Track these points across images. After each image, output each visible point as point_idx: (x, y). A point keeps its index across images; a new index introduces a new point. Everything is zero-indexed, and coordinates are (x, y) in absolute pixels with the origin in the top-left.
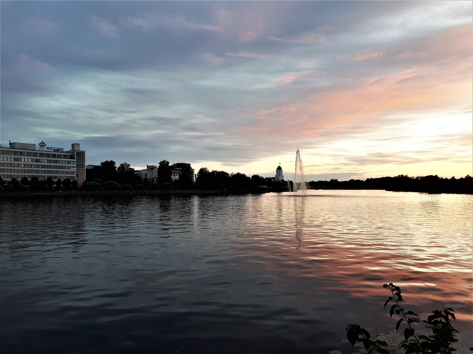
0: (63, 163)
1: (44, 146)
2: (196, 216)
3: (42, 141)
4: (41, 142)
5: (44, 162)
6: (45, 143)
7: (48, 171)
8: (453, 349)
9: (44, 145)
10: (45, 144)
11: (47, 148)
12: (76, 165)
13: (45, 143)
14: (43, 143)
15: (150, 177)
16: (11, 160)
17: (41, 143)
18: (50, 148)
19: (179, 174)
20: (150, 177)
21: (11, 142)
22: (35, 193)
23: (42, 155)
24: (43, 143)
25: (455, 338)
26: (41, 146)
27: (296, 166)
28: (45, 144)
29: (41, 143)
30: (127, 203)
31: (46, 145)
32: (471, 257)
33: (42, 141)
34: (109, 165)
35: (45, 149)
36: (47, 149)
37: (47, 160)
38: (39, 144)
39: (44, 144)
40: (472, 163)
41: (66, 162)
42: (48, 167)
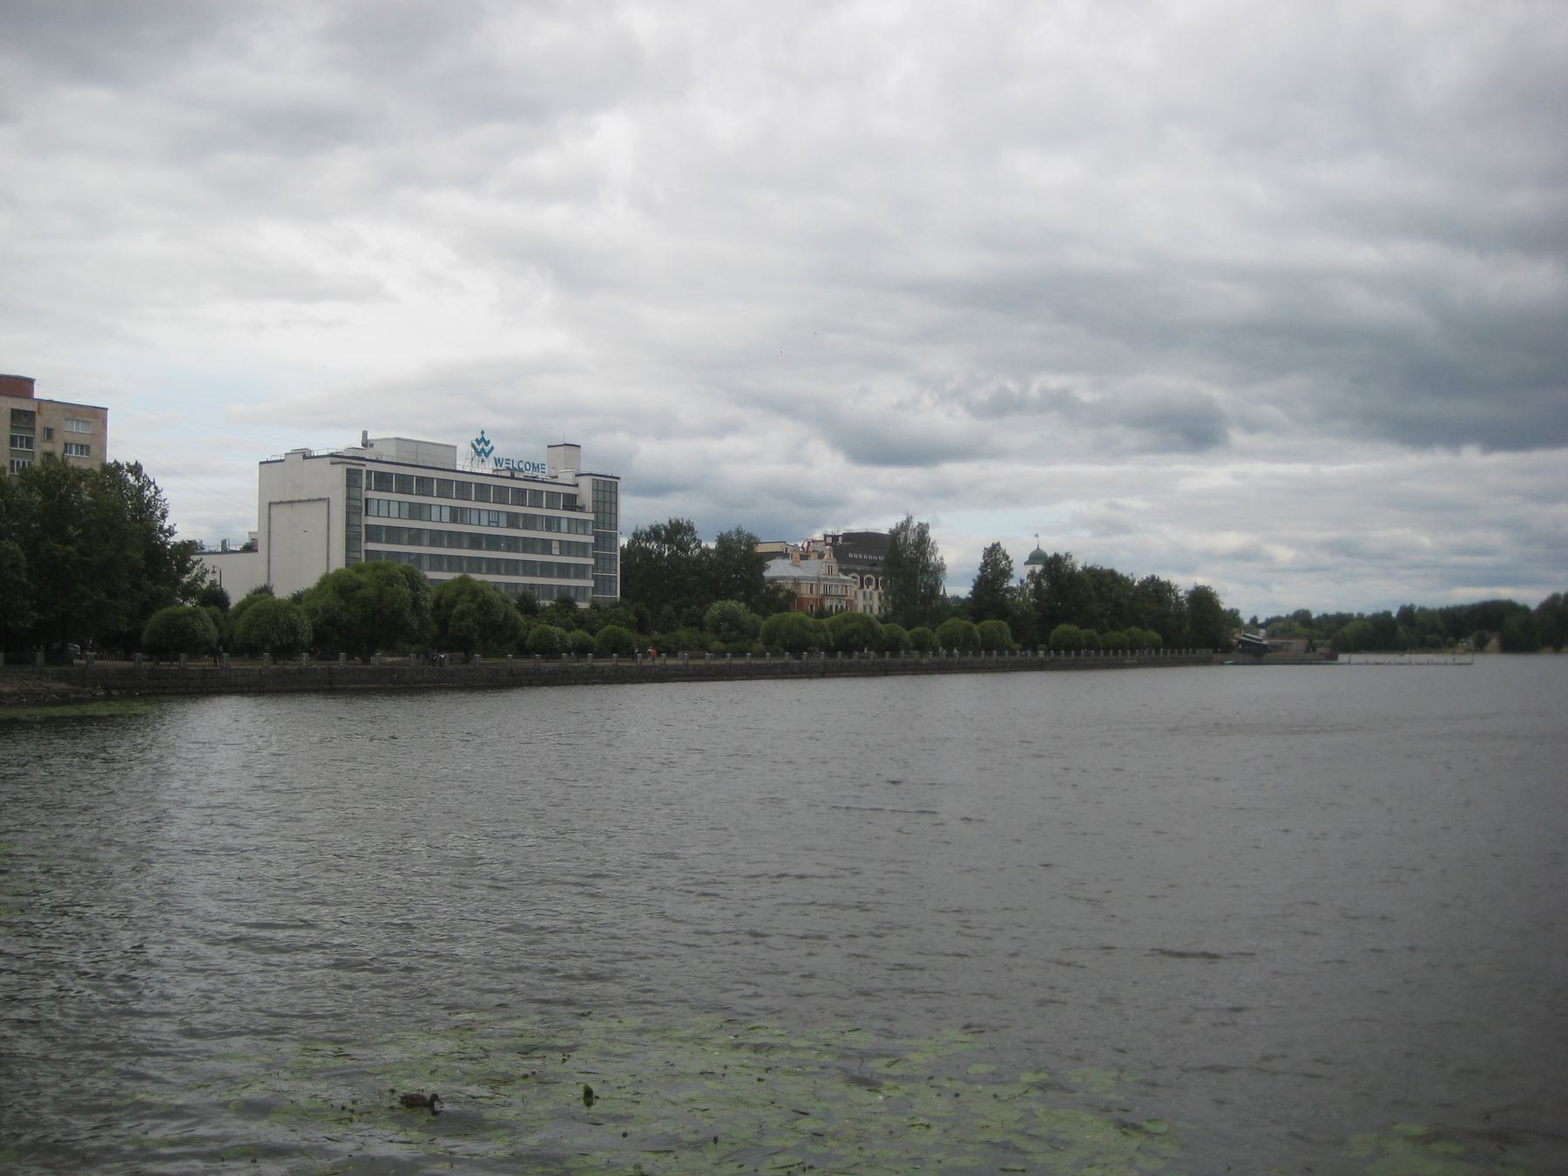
0: (579, 532)
1: (487, 455)
3: (483, 433)
4: (479, 437)
5: (498, 524)
9: (487, 449)
10: (490, 446)
11: (497, 461)
12: (591, 539)
14: (483, 439)
15: (811, 592)
16: (399, 508)
17: (479, 442)
19: (859, 578)
20: (811, 592)
23: (483, 491)
26: (478, 454)
27: (309, 500)
28: (490, 446)
30: (80, 726)
31: (492, 448)
32: (2, 838)
33: (483, 433)
37: (448, 509)
38: (473, 446)
39: (487, 443)
41: (503, 520)
42: (493, 542)
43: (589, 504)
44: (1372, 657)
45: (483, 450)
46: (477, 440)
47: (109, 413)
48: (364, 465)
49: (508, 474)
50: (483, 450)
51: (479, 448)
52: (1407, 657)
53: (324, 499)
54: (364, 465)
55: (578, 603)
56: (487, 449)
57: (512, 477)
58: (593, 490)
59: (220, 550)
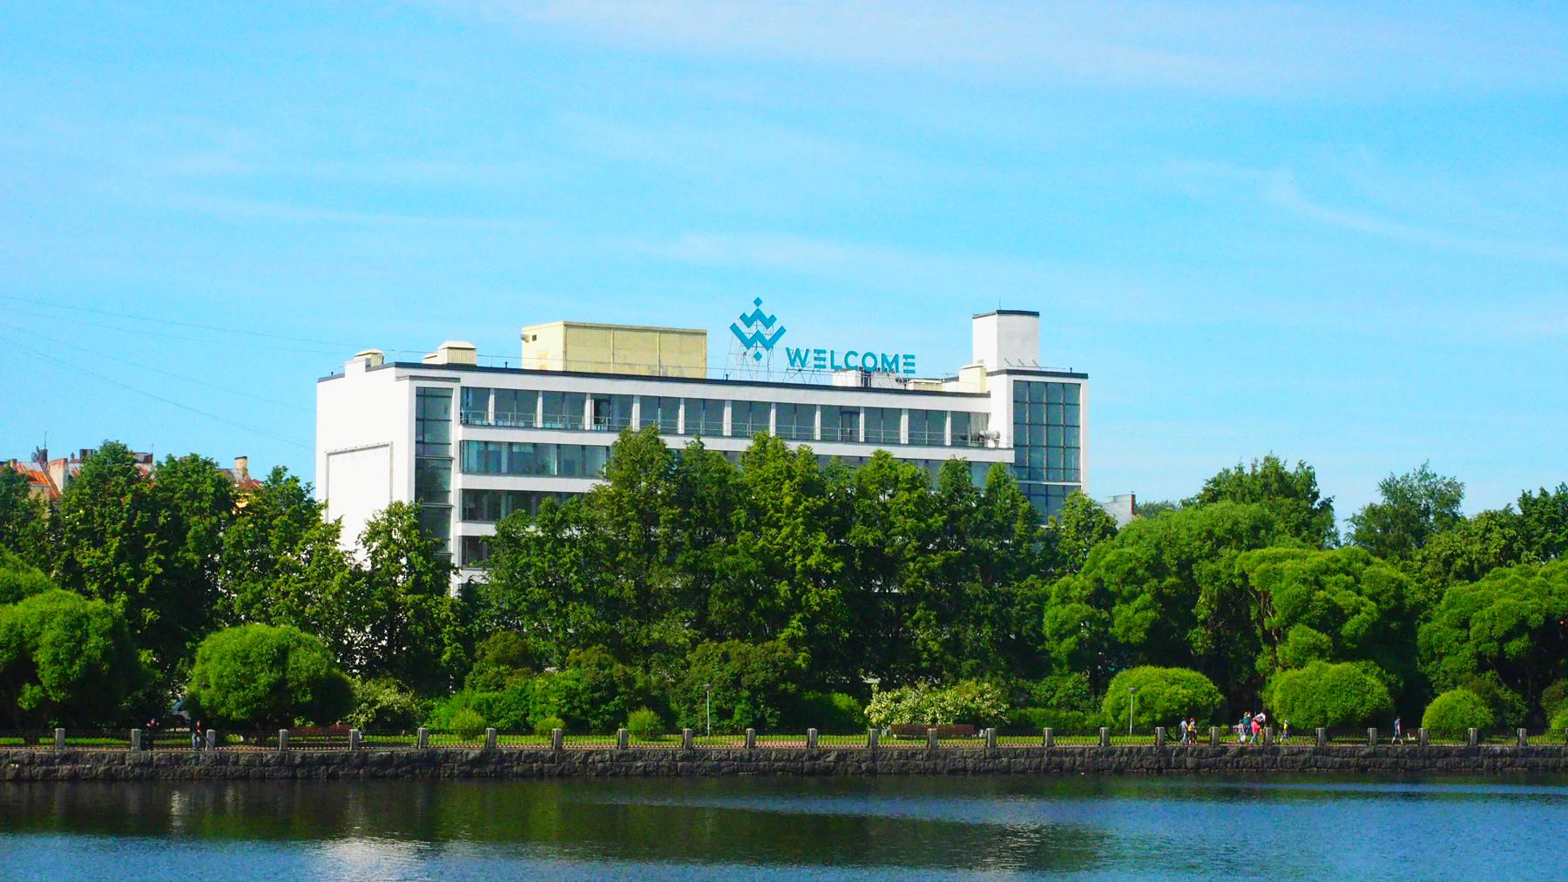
1: (768, 345)
2: (1172, 785)
3: (758, 302)
6: (773, 318)
7: (542, 471)
8: (1135, 509)
9: (768, 334)
10: (776, 327)
11: (795, 357)
13: (773, 318)
14: (758, 315)
18: (812, 355)
21: (1140, 502)
22: (399, 734)
24: (758, 315)
25: (1539, 492)
26: (748, 343)
28: (776, 327)
29: (748, 321)
31: (782, 331)
33: (758, 302)
34: (1167, 668)
35: (776, 366)
36: (792, 362)
38: (734, 328)
39: (769, 322)
40: (1013, 452)
43: (1006, 440)
44: (547, 325)
45: (758, 336)
46: (743, 317)
47: (1087, 396)
48: (457, 380)
49: (852, 379)
50: (758, 336)
51: (750, 332)
52: (542, 326)
53: (387, 445)
54: (457, 380)
55: (871, 833)
56: (768, 334)
57: (866, 388)
58: (417, 419)
59: (907, 442)
